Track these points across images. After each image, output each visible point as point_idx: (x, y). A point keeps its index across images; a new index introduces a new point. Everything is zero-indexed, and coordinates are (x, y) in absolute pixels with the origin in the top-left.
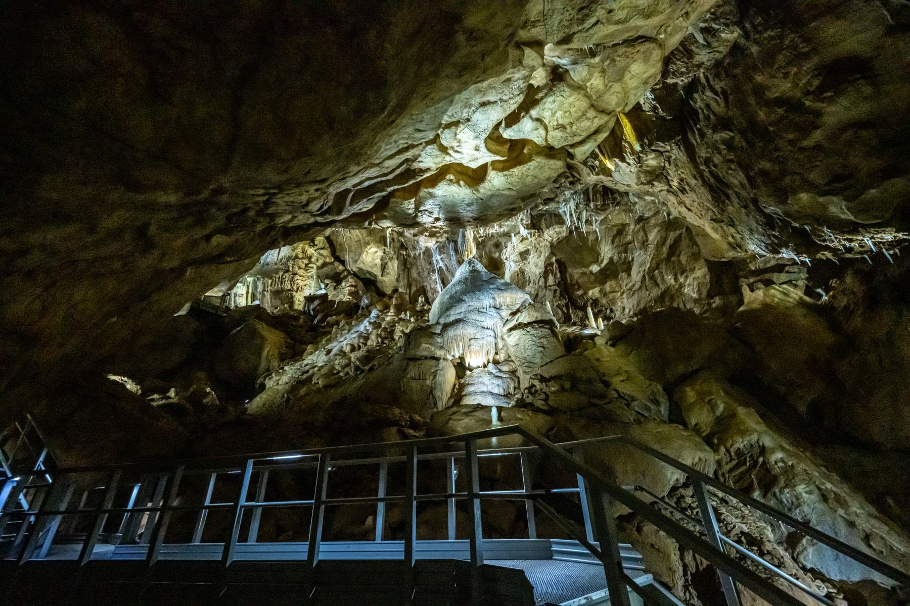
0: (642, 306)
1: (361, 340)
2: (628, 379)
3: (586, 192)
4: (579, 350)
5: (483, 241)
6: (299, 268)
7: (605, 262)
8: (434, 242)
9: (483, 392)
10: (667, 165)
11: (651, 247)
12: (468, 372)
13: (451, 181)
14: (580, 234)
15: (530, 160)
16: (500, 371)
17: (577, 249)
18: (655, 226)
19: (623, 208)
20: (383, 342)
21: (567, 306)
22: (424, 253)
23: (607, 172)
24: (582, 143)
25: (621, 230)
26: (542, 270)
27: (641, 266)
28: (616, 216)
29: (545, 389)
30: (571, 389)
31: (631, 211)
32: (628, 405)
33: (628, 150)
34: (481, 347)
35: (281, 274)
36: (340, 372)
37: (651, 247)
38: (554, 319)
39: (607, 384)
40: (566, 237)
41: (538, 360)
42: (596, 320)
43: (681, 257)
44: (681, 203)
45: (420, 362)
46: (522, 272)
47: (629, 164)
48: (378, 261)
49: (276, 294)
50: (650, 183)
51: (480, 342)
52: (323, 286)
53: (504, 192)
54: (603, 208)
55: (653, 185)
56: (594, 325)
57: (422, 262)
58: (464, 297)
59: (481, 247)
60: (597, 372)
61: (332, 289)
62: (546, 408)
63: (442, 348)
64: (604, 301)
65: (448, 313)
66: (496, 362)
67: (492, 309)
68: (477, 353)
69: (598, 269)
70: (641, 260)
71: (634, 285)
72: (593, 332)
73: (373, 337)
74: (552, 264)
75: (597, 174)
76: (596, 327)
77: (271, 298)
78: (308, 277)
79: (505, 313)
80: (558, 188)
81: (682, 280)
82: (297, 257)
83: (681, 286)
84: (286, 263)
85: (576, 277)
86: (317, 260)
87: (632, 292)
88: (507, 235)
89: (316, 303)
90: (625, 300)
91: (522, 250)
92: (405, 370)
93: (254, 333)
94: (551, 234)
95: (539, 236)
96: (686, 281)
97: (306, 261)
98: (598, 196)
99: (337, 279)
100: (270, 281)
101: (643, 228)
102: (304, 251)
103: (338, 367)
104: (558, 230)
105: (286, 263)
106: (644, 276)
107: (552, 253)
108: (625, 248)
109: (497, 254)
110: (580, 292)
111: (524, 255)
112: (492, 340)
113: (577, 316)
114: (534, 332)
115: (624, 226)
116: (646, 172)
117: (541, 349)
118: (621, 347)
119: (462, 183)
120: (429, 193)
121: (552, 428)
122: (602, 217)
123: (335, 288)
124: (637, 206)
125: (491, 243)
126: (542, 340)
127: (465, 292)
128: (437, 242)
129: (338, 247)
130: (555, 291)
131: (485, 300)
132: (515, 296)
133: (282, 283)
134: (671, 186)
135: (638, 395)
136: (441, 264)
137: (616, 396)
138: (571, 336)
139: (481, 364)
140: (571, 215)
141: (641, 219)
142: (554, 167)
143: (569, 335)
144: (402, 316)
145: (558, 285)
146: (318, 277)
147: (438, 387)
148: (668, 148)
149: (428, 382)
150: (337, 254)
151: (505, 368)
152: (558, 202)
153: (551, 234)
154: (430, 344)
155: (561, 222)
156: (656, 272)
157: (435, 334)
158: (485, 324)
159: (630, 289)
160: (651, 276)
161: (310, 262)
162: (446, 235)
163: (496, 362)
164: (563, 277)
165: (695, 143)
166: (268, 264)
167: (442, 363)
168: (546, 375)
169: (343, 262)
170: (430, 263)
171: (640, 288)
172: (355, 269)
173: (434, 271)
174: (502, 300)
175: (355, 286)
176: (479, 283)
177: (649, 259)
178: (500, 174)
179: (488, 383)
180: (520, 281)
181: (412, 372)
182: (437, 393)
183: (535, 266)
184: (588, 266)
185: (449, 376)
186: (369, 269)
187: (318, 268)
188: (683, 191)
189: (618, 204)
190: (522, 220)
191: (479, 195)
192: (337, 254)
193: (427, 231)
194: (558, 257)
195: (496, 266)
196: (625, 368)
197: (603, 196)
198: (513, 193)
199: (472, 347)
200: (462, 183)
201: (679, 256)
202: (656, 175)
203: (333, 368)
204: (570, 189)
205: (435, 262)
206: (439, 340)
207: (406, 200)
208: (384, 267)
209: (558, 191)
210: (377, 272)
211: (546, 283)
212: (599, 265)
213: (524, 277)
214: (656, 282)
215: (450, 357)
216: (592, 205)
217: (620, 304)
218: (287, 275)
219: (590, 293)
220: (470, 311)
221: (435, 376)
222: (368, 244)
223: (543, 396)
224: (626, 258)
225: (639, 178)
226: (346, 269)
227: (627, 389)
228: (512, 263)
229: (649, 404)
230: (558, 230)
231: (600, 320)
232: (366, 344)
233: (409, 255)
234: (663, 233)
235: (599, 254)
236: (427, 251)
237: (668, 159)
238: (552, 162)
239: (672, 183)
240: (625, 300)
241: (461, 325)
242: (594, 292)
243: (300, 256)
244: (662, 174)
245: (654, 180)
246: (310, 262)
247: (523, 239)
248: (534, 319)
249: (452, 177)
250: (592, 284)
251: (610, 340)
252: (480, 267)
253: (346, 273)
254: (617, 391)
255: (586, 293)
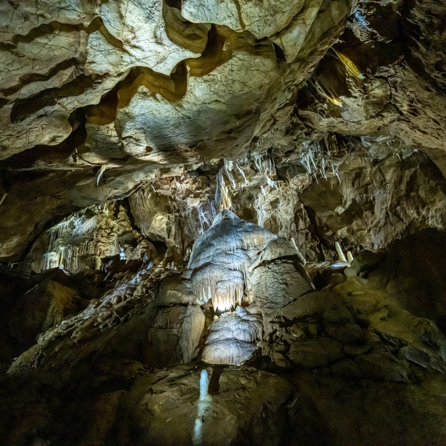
0: (389, 241)
1: (128, 292)
2: (389, 316)
3: (322, 143)
4: (330, 285)
5: (237, 195)
6: (102, 236)
7: (349, 203)
8: (198, 202)
9: (228, 340)
10: (394, 92)
11: (390, 186)
12: (216, 317)
13: (145, 94)
14: (322, 181)
15: (230, 57)
16: (248, 314)
17: (321, 194)
18: (390, 166)
19: (358, 153)
20: (147, 292)
21: (319, 247)
22: (192, 212)
23: (335, 112)
24: (288, 28)
25: (359, 174)
26: (293, 216)
27: (383, 203)
28: (353, 162)
29: (286, 337)
30: (319, 334)
31: (366, 155)
32: (396, 353)
33: (353, 84)
34: (229, 289)
35: (87, 242)
36: (100, 324)
37: (390, 186)
38: (300, 254)
39: (364, 325)
40: (310, 185)
41: (280, 300)
42: (345, 253)
43: (420, 192)
44: (414, 128)
45: (169, 309)
46: (274, 218)
47: (355, 97)
48: (164, 226)
49: (83, 258)
50: (379, 115)
51: (227, 284)
52: (122, 250)
53: (212, 106)
54: (340, 155)
55: (382, 116)
56: (344, 259)
57: (191, 221)
58: (214, 242)
59: (236, 201)
60: (350, 309)
61: (129, 251)
62: (282, 364)
63: (191, 293)
64: (353, 240)
65: (198, 258)
66: (245, 305)
67: (239, 251)
68: (224, 296)
69: (343, 210)
70: (382, 199)
71: (379, 222)
72: (343, 265)
73: (139, 288)
74: (301, 210)
75: (327, 117)
76: (345, 261)
77: (78, 262)
78: (110, 243)
79: (252, 254)
80: (296, 140)
81: (424, 213)
82: (101, 228)
83: (425, 219)
84: (92, 233)
85: (324, 220)
86: (118, 230)
87: (378, 228)
88: (257, 188)
89: (111, 262)
90: (373, 237)
91: (272, 200)
92: (153, 319)
93: (43, 292)
94: (296, 183)
95: (286, 186)
96: (428, 213)
97: (108, 231)
98: (334, 145)
99: (134, 243)
100: (78, 249)
101: (380, 171)
102: (107, 223)
103: (99, 320)
104: (301, 178)
105: (92, 233)
106: (387, 213)
107: (300, 201)
108: (366, 189)
109: (251, 205)
110: (329, 233)
111: (274, 204)
112: (239, 281)
113: (330, 255)
114: (276, 268)
115: (361, 169)
116: (374, 104)
117: (283, 286)
118: (376, 279)
119: (158, 96)
120: (126, 114)
121: (290, 399)
122: (340, 163)
123: (132, 251)
124: (371, 151)
125: (244, 197)
126: (285, 276)
127: (214, 237)
128: (201, 202)
129: (136, 219)
130: (307, 234)
131: (233, 243)
132: (261, 236)
133: (87, 249)
134: (401, 114)
135: (409, 338)
136: (205, 220)
137: (377, 339)
138: (321, 272)
139: (228, 307)
140: (311, 164)
141: (376, 162)
142: (263, 69)
143: (318, 270)
144: (168, 267)
145: (309, 228)
146: (119, 243)
147: (184, 336)
148: (392, 71)
149: (175, 331)
150: (135, 224)
151: (253, 311)
152: (298, 153)
153: (296, 183)
154: (177, 290)
155: (303, 170)
156: (398, 208)
157: (185, 279)
158: (232, 266)
159: (376, 226)
160: (393, 212)
161: (112, 231)
162: (207, 195)
163: (245, 305)
164: (313, 221)
165: (420, 57)
166: (77, 236)
167: (190, 309)
168: (290, 318)
169: (139, 230)
170: (197, 220)
171: (385, 224)
172: (147, 235)
173: (200, 226)
174: (249, 241)
175: (147, 248)
176: (228, 228)
177: (389, 197)
178: (199, 80)
179: (233, 328)
180: (273, 226)
181: (160, 321)
182: (183, 343)
183: (285, 213)
184: (333, 210)
185: (199, 320)
186: (158, 233)
187: (119, 236)
188: (414, 112)
189: (353, 150)
190: (268, 173)
191: (184, 112)
192: (135, 224)
193: (192, 193)
194: (307, 204)
195: (249, 215)
196: (383, 303)
197: (338, 145)
198: (223, 107)
199: (219, 290)
200: (158, 96)
201: (417, 191)
202: (384, 106)
203: (96, 320)
204: (306, 139)
205: (200, 218)
206: (188, 285)
207: (103, 125)
208: (169, 231)
209: (296, 143)
210: (164, 234)
211: (297, 227)
212: (344, 207)
213: (276, 224)
214: (398, 216)
215: (199, 303)
216: (329, 153)
217: (368, 240)
218: (91, 243)
219: (339, 233)
220: (217, 255)
221: (182, 323)
222: (156, 213)
223: (281, 347)
224: (367, 198)
225: (367, 111)
226: (142, 235)
227: (391, 329)
228: (264, 212)
229: (425, 350)
230: (301, 178)
231: (350, 254)
232: (131, 295)
233: (181, 216)
234: (399, 172)
235: (342, 196)
236: (194, 209)
237: (394, 85)
238: (258, 60)
239: (401, 109)
240: (373, 237)
241: (208, 269)
242: (342, 232)
243: (104, 227)
244: (390, 103)
245: (382, 111)
246: (112, 231)
247: (272, 189)
248: (277, 256)
249: (145, 90)
250: (340, 224)
251: (361, 271)
252: (232, 215)
253: (141, 238)
254: (379, 333)
255: (334, 234)
